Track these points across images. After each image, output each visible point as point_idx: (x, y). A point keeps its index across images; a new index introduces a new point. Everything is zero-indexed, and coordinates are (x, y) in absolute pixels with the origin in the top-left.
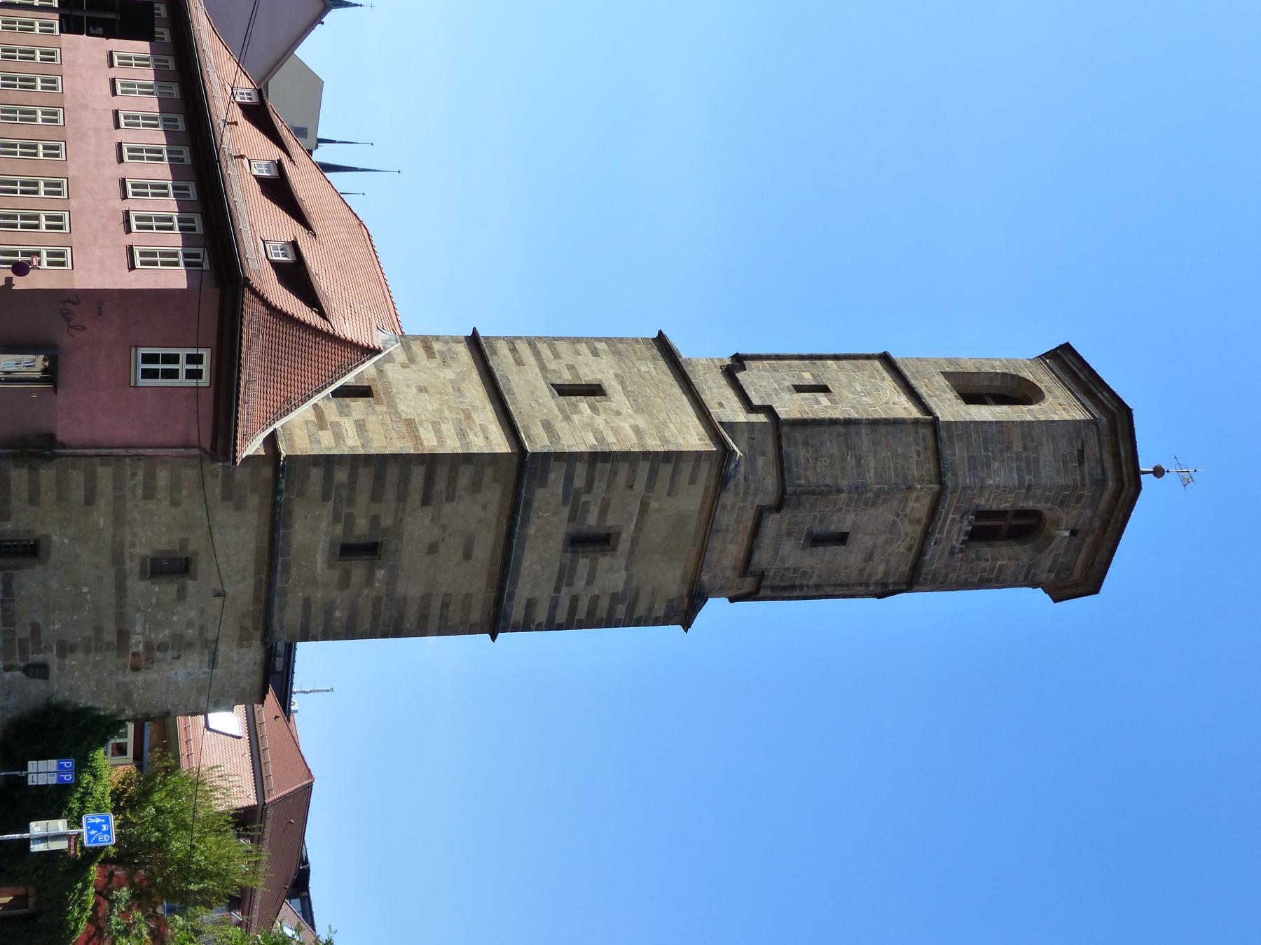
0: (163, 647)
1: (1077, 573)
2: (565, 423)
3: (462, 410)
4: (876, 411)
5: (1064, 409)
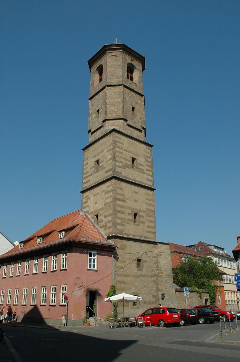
0: (157, 266)
2: (106, 168)
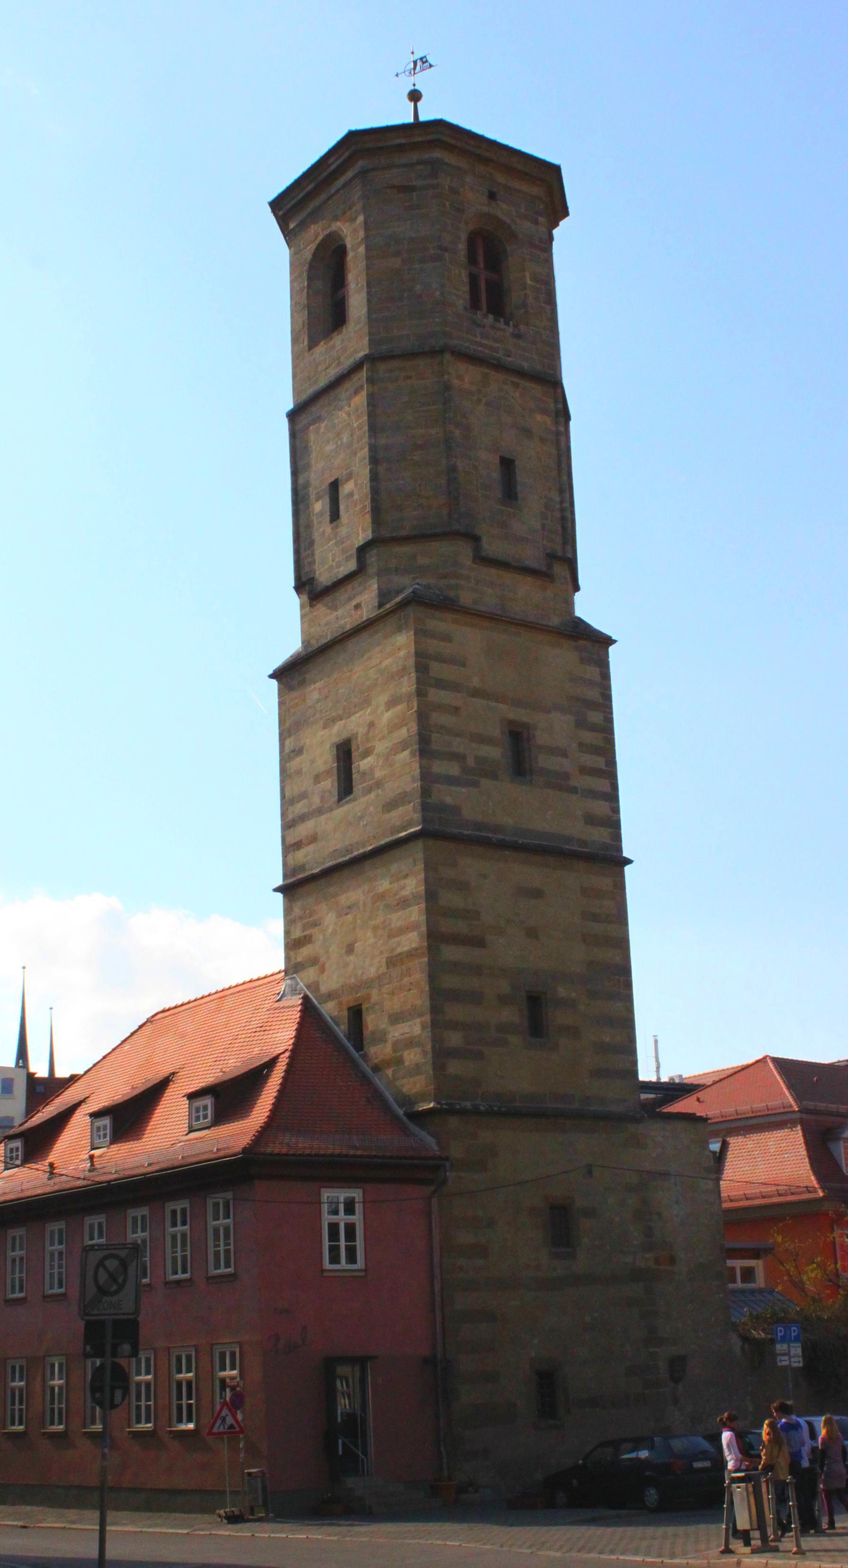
1: (536, 191)
3: (373, 904)
4: (360, 428)
5: (350, 208)
